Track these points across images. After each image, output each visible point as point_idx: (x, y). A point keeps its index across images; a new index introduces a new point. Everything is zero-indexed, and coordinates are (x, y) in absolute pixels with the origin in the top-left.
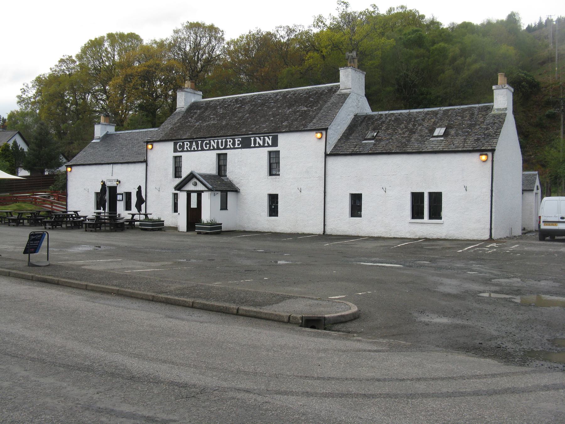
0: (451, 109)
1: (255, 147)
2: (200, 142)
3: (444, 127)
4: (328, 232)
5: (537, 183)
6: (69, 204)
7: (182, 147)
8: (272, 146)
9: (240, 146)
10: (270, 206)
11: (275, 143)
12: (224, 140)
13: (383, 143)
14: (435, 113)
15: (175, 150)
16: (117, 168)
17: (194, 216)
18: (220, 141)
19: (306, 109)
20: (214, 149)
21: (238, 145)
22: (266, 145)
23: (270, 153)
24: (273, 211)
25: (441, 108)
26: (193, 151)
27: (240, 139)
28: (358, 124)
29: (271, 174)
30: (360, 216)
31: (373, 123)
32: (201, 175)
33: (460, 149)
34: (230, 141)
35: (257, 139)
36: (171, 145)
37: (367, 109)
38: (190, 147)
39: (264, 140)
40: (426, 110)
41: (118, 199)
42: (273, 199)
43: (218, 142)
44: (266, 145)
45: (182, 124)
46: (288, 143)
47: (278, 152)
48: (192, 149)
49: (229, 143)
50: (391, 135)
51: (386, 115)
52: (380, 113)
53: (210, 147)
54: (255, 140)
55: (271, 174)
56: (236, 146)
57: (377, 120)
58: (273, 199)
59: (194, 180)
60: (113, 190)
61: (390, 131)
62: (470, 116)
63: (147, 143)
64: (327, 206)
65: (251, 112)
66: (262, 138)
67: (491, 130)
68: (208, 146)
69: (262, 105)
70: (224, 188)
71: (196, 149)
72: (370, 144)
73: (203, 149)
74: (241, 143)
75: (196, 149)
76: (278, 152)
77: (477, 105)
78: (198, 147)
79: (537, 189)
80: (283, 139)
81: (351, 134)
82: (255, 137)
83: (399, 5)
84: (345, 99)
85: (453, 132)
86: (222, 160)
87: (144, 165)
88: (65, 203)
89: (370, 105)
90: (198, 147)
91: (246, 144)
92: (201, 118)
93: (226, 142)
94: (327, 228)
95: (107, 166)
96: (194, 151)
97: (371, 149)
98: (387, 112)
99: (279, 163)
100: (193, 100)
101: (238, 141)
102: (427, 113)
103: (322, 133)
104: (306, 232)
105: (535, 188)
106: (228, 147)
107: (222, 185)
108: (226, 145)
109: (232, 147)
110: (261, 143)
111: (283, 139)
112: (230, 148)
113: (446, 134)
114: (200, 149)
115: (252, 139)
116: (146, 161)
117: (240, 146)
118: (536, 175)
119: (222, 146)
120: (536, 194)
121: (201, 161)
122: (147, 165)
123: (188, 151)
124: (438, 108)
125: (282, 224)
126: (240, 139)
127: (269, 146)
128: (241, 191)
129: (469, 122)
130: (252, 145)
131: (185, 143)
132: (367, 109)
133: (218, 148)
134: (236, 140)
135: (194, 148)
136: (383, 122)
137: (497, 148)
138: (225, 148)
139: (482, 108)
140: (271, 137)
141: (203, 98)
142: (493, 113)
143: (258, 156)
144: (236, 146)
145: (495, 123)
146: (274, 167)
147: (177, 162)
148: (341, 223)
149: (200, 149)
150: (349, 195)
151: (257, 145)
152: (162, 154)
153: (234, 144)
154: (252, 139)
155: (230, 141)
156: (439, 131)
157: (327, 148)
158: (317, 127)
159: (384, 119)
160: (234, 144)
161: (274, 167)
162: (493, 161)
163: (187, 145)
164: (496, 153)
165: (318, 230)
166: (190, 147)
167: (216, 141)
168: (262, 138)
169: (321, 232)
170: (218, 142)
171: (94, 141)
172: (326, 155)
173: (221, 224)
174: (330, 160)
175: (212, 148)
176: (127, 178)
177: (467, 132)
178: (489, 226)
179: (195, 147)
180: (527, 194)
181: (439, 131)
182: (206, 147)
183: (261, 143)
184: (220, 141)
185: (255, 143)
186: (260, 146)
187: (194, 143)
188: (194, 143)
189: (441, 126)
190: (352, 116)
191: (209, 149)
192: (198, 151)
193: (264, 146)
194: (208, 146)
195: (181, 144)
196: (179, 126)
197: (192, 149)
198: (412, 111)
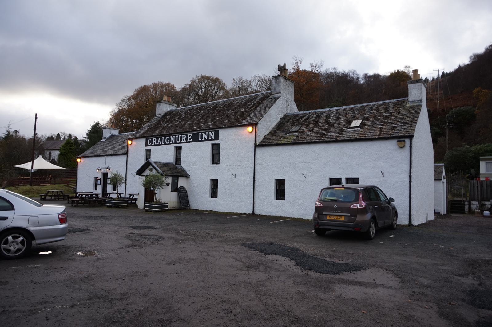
0: (366, 105)
1: (202, 141)
2: (163, 138)
3: (361, 119)
4: (257, 212)
5: (444, 174)
6: (78, 186)
7: (151, 142)
8: (214, 140)
9: (191, 140)
10: (212, 189)
11: (216, 137)
12: (180, 136)
13: (305, 135)
14: (352, 109)
15: (147, 145)
16: (109, 158)
17: (149, 195)
18: (177, 136)
19: (244, 110)
20: (173, 143)
21: (190, 139)
22: (210, 139)
23: (213, 145)
24: (214, 194)
25: (358, 105)
26: (153, 145)
27: (191, 135)
28: (286, 121)
29: (213, 163)
30: (284, 200)
31: (298, 120)
32: (155, 163)
33: (377, 137)
34: (184, 137)
35: (204, 134)
36: (143, 141)
37: (295, 110)
38: (157, 142)
39: (209, 134)
40: (344, 107)
41: (108, 182)
42: (214, 183)
43: (175, 138)
44: (210, 139)
45: (155, 126)
46: (227, 136)
47: (219, 144)
48: (158, 144)
49: (183, 138)
50: (313, 128)
51: (309, 113)
52: (305, 112)
53: (170, 141)
54: (202, 135)
55: (213, 163)
56: (188, 140)
57: (301, 117)
58: (214, 183)
59: (151, 167)
60: (105, 175)
61: (312, 125)
62: (385, 109)
63: (129, 139)
64: (256, 189)
65: (204, 114)
66: (207, 133)
67: (407, 119)
68: (169, 141)
69: (213, 109)
70: (174, 174)
71: (160, 144)
72: (293, 136)
73: (165, 144)
74: (192, 137)
75: (160, 144)
76: (219, 144)
77: (392, 101)
78: (162, 142)
79: (444, 179)
80: (223, 133)
81: (279, 129)
82: (202, 133)
83: (333, 67)
84: (276, 101)
85: (369, 122)
86: (178, 150)
87: (125, 156)
88: (75, 185)
89: (298, 106)
90: (162, 142)
91: (195, 139)
92: (170, 121)
93: (181, 137)
94: (256, 209)
95: (103, 157)
96: (159, 145)
97: (295, 140)
98: (310, 111)
99: (219, 154)
100: (169, 109)
101: (190, 136)
102: (345, 110)
103: (253, 127)
104: (239, 212)
105: (443, 178)
106: (183, 141)
107: (176, 171)
108: (181, 140)
109: (185, 141)
110: (206, 137)
111: (223, 133)
112: (184, 142)
113: (362, 125)
114: (163, 143)
115: (200, 134)
116: (127, 154)
117: (191, 140)
118: (442, 166)
119: (178, 141)
120: (443, 182)
121: (163, 154)
122: (127, 156)
123: (155, 145)
124: (356, 105)
125: (218, 205)
126: (191, 135)
127: (212, 140)
128: (191, 177)
129: (384, 114)
130: (200, 139)
131: (154, 139)
132: (294, 109)
133: (176, 143)
134: (188, 135)
135: (159, 143)
136: (307, 119)
137: (415, 135)
138: (181, 143)
139: (396, 103)
140: (213, 132)
141: (177, 108)
142: (408, 105)
143: (204, 148)
144: (188, 140)
145: (411, 113)
146: (215, 159)
147: (148, 151)
148: (269, 206)
149: (163, 143)
150: (274, 180)
151: (203, 139)
152: (137, 148)
153: (187, 139)
154: (200, 134)
155: (184, 137)
156: (356, 123)
157: (257, 139)
158: (250, 122)
159: (307, 116)
160: (187, 139)
161: (215, 159)
162: (411, 147)
163: (155, 140)
164: (414, 140)
165: (248, 210)
166: (157, 142)
167: (174, 137)
168: (207, 133)
169: (251, 213)
170: (175, 138)
171: (102, 140)
172: (256, 146)
173: (167, 203)
174: (259, 150)
175: (171, 142)
176: (115, 165)
177: (383, 122)
178: (408, 212)
179: (160, 142)
180: (438, 182)
181: (356, 123)
182: (168, 142)
183: (206, 137)
184: (177, 136)
185: (202, 138)
186: (206, 140)
187: (159, 139)
188: (159, 139)
189: (357, 119)
190: (282, 116)
191: (170, 144)
192: (162, 145)
193: (208, 140)
194: (169, 141)
195: (151, 139)
196: (153, 127)
197: (158, 144)
198: (331, 109)
